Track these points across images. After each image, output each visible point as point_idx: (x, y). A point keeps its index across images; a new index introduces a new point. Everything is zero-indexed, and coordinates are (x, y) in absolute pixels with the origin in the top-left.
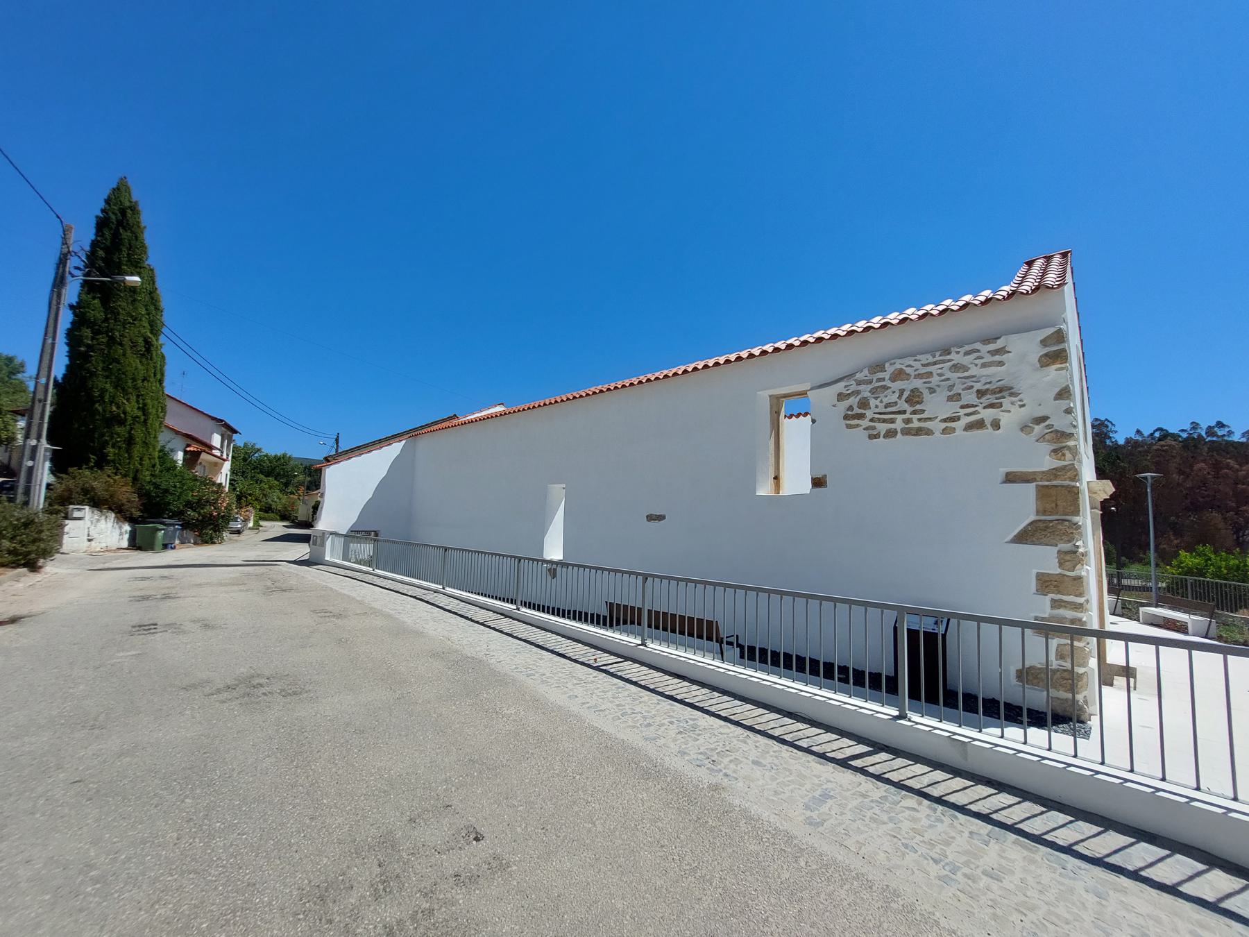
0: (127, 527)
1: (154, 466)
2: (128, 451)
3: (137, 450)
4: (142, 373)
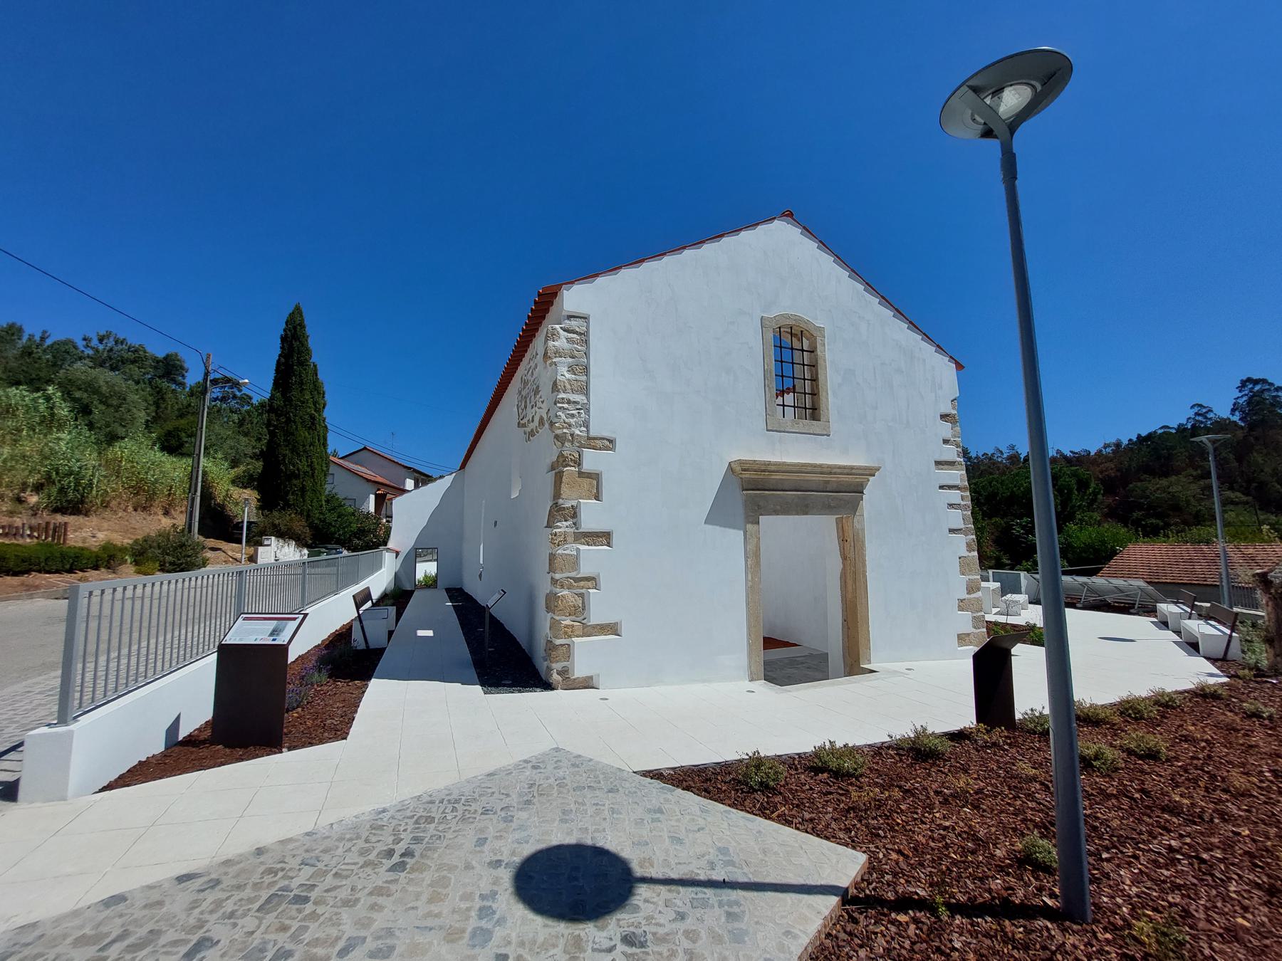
2: (303, 496)
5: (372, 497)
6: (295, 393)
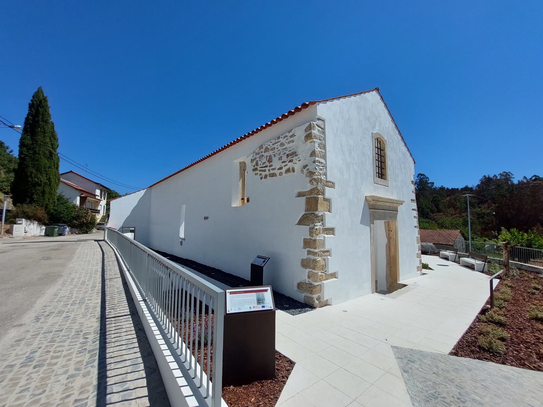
0: (44, 227)
1: (54, 202)
2: (43, 196)
3: (47, 196)
4: (48, 165)
5: (78, 198)
6: (40, 138)
